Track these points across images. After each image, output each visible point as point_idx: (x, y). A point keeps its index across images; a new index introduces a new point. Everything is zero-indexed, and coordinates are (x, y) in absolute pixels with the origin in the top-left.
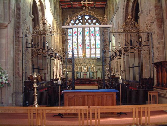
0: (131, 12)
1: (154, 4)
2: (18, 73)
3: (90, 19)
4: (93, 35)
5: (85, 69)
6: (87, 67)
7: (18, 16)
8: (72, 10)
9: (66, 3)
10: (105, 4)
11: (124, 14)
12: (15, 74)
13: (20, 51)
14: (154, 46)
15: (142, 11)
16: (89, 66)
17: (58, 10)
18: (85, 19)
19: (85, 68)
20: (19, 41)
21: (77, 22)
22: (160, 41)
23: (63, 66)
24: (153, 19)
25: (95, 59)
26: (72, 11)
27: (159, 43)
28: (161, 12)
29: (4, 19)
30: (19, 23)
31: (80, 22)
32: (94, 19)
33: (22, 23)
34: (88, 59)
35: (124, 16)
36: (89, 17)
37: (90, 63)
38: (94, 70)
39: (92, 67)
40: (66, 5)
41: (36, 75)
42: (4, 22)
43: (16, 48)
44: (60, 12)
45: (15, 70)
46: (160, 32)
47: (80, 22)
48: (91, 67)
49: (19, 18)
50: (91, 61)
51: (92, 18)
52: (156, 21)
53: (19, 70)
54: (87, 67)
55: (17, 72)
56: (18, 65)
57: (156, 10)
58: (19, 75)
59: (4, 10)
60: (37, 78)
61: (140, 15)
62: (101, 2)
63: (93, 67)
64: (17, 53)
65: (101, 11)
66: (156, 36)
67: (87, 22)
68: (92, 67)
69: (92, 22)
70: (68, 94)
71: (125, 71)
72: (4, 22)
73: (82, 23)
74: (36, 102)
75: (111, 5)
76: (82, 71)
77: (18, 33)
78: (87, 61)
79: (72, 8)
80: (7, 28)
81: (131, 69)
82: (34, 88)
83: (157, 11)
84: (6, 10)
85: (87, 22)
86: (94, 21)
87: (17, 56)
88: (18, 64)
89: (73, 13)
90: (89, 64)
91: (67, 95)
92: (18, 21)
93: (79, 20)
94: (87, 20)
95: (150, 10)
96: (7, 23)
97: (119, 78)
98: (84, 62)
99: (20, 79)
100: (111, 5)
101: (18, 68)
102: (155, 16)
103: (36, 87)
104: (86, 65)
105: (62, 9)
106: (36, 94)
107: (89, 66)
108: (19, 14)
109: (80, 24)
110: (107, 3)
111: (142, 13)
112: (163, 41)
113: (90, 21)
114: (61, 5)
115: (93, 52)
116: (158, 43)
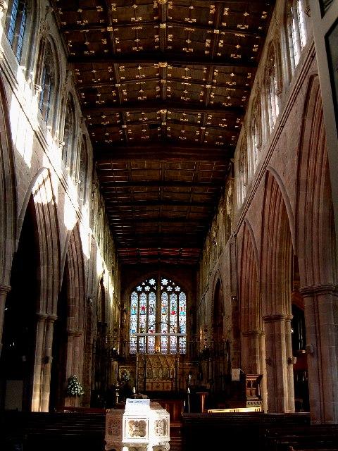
2: (88, 381)
3: (169, 284)
4: (174, 313)
18: (162, 285)
21: (147, 288)
31: (152, 290)
34: (164, 356)
36: (168, 281)
47: (152, 290)
48: (169, 370)
50: (169, 360)
63: (173, 371)
67: (165, 290)
69: (173, 290)
73: (155, 292)
78: (162, 360)
85: (165, 290)
86: (178, 289)
88: (88, 372)
94: (165, 287)
113: (169, 289)
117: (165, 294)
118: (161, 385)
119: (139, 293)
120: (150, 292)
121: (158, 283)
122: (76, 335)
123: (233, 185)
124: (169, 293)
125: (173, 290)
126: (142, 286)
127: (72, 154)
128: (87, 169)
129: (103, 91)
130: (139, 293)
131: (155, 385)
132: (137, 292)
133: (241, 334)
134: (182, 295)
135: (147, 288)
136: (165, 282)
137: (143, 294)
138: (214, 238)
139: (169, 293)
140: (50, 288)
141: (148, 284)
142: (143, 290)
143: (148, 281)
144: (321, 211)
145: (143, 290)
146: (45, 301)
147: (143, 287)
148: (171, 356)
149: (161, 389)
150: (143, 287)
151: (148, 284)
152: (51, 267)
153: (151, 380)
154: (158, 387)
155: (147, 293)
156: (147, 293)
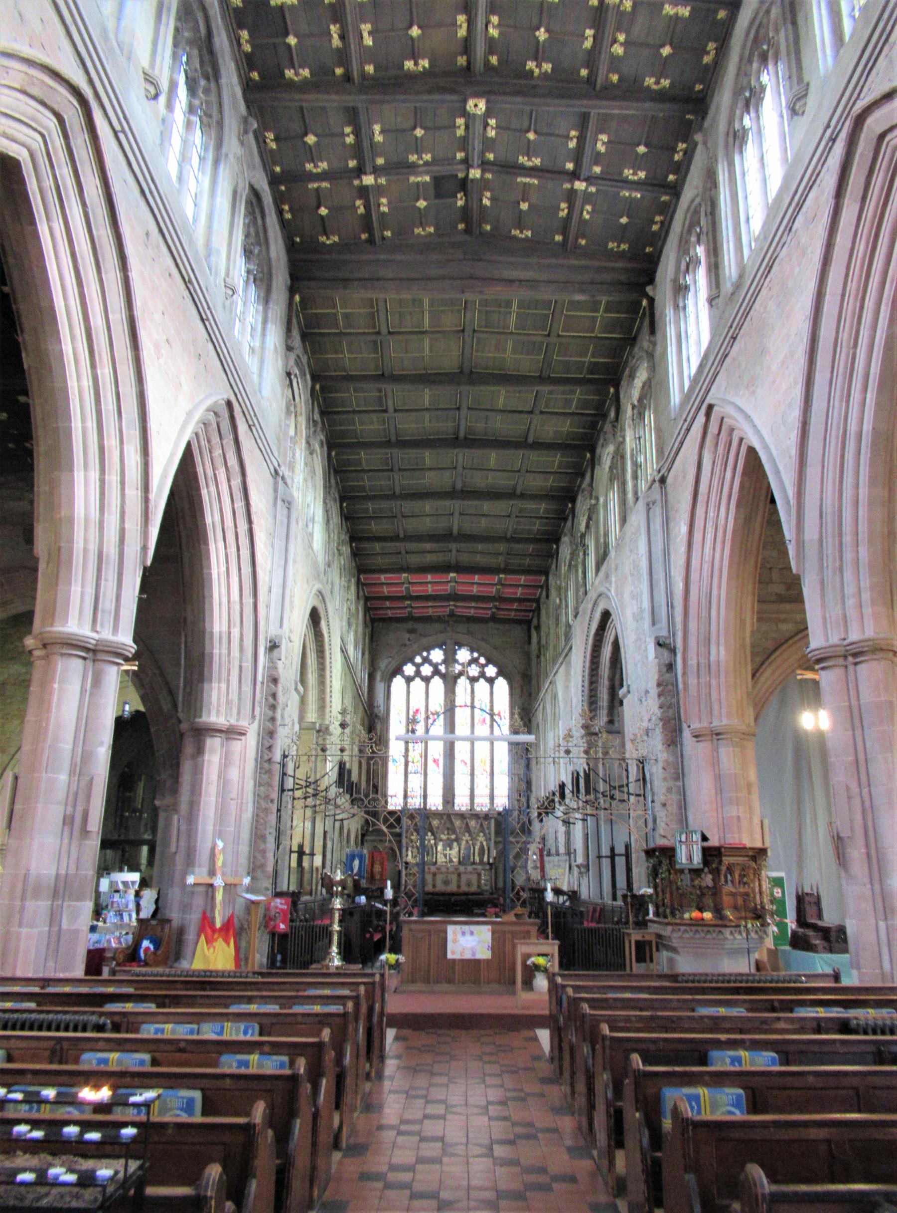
0: (607, 670)
1: (656, 677)
2: (263, 866)
5: (454, 853)
6: (459, 845)
7: (271, 700)
8: (410, 625)
9: (382, 577)
10: (533, 611)
11: (587, 677)
12: (253, 869)
13: (272, 801)
14: (656, 798)
15: (628, 686)
16: (464, 843)
17: (360, 629)
18: (456, 661)
19: (448, 852)
20: (269, 772)
21: (426, 670)
22: (671, 783)
23: (367, 838)
24: (654, 718)
25: (487, 817)
26: (410, 631)
27: (669, 790)
28: (674, 701)
29: (239, 713)
30: (273, 719)
31: (436, 672)
32: (489, 661)
33: (279, 721)
34: (462, 816)
35: (586, 684)
37: (468, 829)
38: (485, 859)
39: (477, 848)
40: (382, 584)
41: (343, 873)
42: (238, 720)
43: (262, 795)
44: (364, 634)
45: (254, 857)
46: (671, 759)
47: (436, 672)
48: (474, 846)
49: (273, 707)
50: (473, 823)
51: (482, 660)
52: (661, 724)
53: (264, 857)
54: (459, 845)
55: (258, 863)
56: (265, 842)
57: (659, 696)
58: (263, 872)
59: (240, 687)
60: (343, 884)
61: (625, 696)
62: (523, 578)
63: (482, 848)
64: (264, 805)
65: (518, 632)
66: (660, 770)
68: (477, 848)
69: (482, 675)
70: (413, 926)
71: (587, 867)
72: (238, 720)
73: (443, 676)
74: (335, 949)
75: (552, 622)
76: (439, 860)
77: (270, 748)
78: (457, 823)
79: (411, 618)
80: (243, 738)
81: (606, 863)
82: (333, 909)
83: (662, 699)
84: (244, 688)
86: (491, 671)
87: (262, 815)
88: (263, 838)
89: (412, 636)
90: (467, 837)
91: (410, 930)
92: (270, 713)
93: (435, 666)
95: (647, 692)
96: (244, 723)
97: (545, 889)
98: (448, 825)
99: (264, 885)
100: (552, 622)
101: (264, 851)
102: (658, 713)
103: (339, 906)
104: (453, 837)
105: (373, 621)
106: (336, 927)
107: (464, 843)
108: (274, 696)
109: (437, 678)
110: (538, 608)
111: (629, 692)
112: (680, 784)
113: (474, 671)
114: (364, 584)
115: (482, 791)
116: (664, 790)
117: (463, 682)
118: (454, 878)
119: (409, 680)
120: (432, 677)
121: (450, 659)
122: (232, 733)
123: (651, 355)
124: (473, 680)
125: (482, 675)
126: (414, 664)
127: (210, 227)
128: (220, 124)
129: (297, 127)
130: (409, 680)
131: (439, 878)
132: (404, 676)
133: (687, 734)
134: (502, 685)
135: (426, 670)
136: (463, 655)
137: (418, 680)
138: (583, 536)
139: (473, 680)
140: (111, 549)
141: (426, 660)
142: (418, 673)
143: (429, 654)
144: (867, 427)
145: (418, 673)
146: (90, 590)
147: (418, 666)
148: (476, 816)
149: (452, 888)
150: (418, 666)
151: (426, 660)
152: (113, 478)
153: (433, 869)
154: (446, 883)
155: (427, 680)
156: (427, 680)
